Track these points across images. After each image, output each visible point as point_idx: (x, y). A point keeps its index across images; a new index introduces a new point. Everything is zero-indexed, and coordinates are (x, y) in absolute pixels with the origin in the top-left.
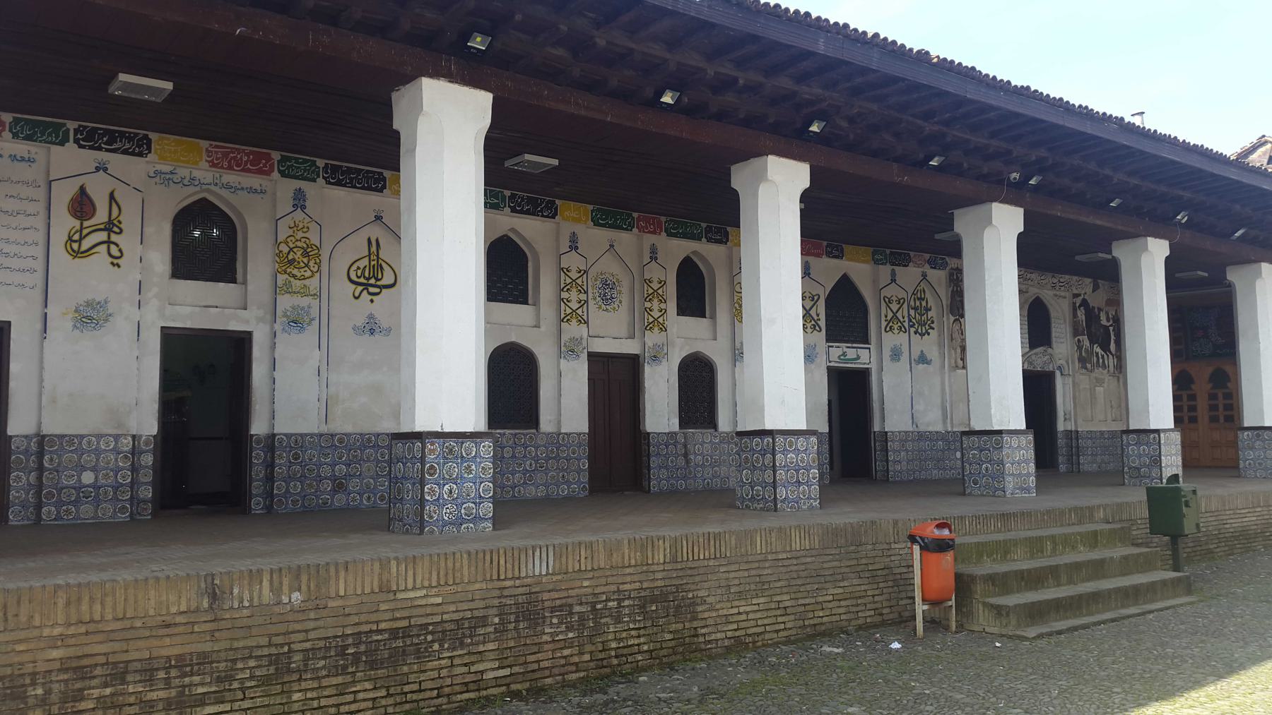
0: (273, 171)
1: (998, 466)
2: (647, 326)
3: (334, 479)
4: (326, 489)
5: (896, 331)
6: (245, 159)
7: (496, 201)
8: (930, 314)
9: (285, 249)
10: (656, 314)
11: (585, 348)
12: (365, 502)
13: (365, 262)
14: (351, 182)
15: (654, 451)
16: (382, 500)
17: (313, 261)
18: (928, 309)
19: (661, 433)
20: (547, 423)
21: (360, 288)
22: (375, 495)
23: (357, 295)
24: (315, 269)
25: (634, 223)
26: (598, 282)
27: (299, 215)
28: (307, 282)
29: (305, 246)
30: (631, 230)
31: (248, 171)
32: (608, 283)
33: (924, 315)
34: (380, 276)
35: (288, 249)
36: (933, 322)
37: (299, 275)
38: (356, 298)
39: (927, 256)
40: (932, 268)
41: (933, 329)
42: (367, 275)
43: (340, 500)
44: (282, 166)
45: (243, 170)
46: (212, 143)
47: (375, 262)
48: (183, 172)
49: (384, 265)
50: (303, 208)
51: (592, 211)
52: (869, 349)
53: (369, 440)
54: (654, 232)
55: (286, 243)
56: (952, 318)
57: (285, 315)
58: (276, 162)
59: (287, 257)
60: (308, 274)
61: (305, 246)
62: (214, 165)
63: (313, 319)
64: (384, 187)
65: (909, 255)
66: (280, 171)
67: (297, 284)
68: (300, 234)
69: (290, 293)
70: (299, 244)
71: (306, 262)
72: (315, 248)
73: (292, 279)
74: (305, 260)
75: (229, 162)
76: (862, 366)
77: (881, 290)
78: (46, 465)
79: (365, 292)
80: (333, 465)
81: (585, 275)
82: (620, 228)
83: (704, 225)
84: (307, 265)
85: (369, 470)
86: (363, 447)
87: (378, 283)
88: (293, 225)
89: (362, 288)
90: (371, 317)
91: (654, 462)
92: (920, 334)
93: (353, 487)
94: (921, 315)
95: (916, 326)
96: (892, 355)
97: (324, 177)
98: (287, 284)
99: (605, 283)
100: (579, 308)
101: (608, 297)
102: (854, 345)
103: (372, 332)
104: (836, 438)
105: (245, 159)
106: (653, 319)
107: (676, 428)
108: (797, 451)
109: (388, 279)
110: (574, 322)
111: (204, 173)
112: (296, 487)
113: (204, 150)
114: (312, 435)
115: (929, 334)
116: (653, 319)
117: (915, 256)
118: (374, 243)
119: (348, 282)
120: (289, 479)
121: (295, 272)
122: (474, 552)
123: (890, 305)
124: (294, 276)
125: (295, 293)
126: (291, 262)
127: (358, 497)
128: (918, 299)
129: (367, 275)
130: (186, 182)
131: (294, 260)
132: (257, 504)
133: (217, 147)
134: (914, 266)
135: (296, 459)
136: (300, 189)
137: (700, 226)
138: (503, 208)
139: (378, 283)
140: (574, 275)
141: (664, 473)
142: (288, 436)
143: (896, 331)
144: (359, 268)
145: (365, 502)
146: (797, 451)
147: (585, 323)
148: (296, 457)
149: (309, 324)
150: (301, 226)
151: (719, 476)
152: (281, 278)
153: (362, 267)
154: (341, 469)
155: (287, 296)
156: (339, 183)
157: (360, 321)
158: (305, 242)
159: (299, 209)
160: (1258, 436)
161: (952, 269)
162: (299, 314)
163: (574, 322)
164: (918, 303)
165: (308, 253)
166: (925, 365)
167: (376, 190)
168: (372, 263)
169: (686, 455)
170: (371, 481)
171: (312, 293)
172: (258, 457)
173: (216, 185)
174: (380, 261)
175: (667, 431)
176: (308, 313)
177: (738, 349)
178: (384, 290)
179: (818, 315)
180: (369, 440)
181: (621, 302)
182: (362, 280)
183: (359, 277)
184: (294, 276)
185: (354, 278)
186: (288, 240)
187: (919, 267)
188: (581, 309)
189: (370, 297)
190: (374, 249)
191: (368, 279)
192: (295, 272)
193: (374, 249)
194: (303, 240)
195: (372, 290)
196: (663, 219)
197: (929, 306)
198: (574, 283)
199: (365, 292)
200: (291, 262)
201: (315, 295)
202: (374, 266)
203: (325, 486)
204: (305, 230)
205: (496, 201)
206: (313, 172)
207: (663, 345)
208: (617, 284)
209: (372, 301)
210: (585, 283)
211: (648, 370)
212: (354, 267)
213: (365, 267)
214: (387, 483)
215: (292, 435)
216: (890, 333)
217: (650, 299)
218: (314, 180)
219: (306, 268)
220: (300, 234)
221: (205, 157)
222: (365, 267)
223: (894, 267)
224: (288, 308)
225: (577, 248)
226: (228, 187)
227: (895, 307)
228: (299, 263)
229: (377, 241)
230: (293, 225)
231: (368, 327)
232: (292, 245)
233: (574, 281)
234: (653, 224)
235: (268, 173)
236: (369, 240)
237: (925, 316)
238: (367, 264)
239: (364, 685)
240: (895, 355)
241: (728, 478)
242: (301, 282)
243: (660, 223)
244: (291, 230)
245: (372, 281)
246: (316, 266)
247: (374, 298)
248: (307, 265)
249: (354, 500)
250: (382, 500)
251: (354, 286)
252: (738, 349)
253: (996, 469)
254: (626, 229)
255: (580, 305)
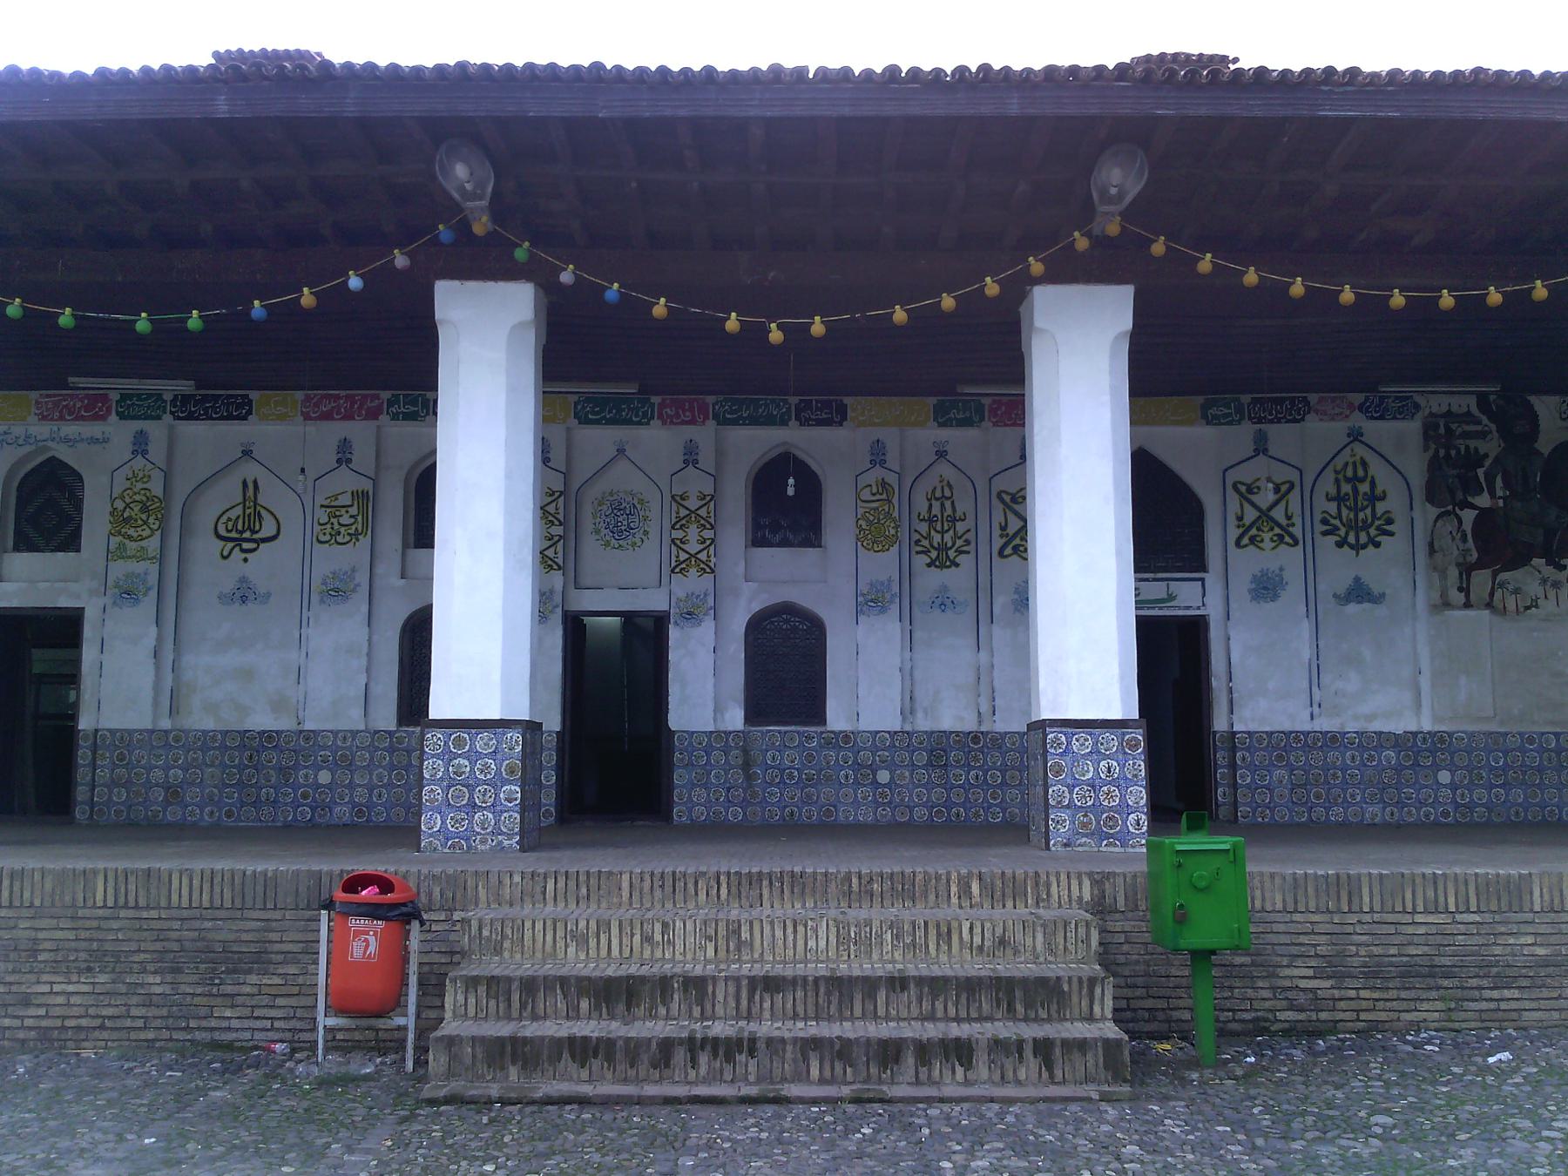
0: (110, 414)
1: (322, 810)
2: (676, 566)
3: (167, 788)
4: (157, 799)
5: (1267, 544)
6: (79, 405)
7: (413, 409)
8: (1381, 507)
9: (120, 505)
10: (693, 547)
11: (557, 606)
12: (206, 818)
13: (238, 511)
14: (206, 413)
15: (682, 760)
16: (229, 817)
17: (154, 516)
18: (1374, 498)
19: (1009, 733)
20: (837, 718)
21: (230, 545)
22: (220, 810)
23: (225, 553)
24: (155, 527)
25: (653, 411)
26: (605, 507)
27: (139, 462)
28: (143, 543)
29: (144, 499)
30: (648, 424)
31: (83, 418)
32: (622, 507)
33: (1363, 509)
34: (257, 528)
35: (124, 505)
36: (1390, 522)
37: (135, 535)
38: (225, 558)
39: (1358, 398)
40: (1373, 418)
41: (1391, 534)
42: (240, 528)
43: (173, 814)
44: (121, 407)
45: (76, 419)
46: (42, 392)
47: (252, 510)
48: (18, 430)
49: (263, 512)
50: (144, 453)
51: (576, 404)
52: (1202, 580)
53: (214, 739)
54: (693, 422)
55: (122, 498)
56: (1434, 512)
57: (117, 586)
58: (114, 405)
59: (122, 515)
60: (147, 532)
61: (144, 499)
62: (44, 418)
63: (149, 589)
64: (250, 412)
65: (1305, 400)
66: (118, 413)
67: (132, 546)
68: (140, 485)
69: (123, 558)
70: (137, 498)
71: (145, 519)
72: (156, 500)
73: (127, 542)
74: (144, 517)
75: (61, 412)
76: (1181, 613)
77: (1226, 470)
78: (1239, 762)
79: (237, 549)
80: (167, 768)
81: (712, 503)
82: (628, 422)
83: (794, 400)
84: (145, 523)
85: (213, 777)
86: (205, 749)
87: (255, 536)
88: (130, 476)
89: (233, 544)
90: (243, 580)
91: (680, 777)
92: (1351, 547)
93: (192, 799)
94: (1356, 509)
95: (1342, 532)
96: (1254, 590)
97: (172, 413)
98: (121, 546)
99: (617, 508)
100: (550, 547)
101: (623, 528)
102: (1160, 575)
103: (244, 599)
104: (567, 737)
105: (79, 405)
106: (687, 556)
107: (735, 718)
108: (474, 756)
109: (268, 529)
110: (693, 571)
111: (42, 430)
112: (120, 795)
113: (34, 402)
114: (141, 732)
115: (1377, 545)
116: (687, 556)
117: (1320, 400)
118: (251, 486)
119: (213, 536)
120: (114, 783)
121: (131, 532)
122: (1461, 879)
123: (1253, 498)
124: (130, 537)
125: (130, 557)
126: (127, 521)
127: (198, 811)
128: (1348, 480)
129: (240, 528)
130: (21, 442)
131: (130, 518)
132: (80, 813)
133: (48, 396)
134: (1321, 420)
135: (121, 760)
136: (142, 432)
137: (785, 402)
138: (424, 417)
139: (255, 536)
140: (693, 503)
141: (700, 794)
142: (112, 732)
143: (1267, 544)
144: (230, 520)
145: (206, 818)
146: (474, 756)
147: (560, 568)
148: (121, 758)
149: (145, 594)
150: (141, 475)
151: (816, 802)
152: (115, 540)
153: (234, 518)
154: (176, 774)
155: (121, 562)
156: (191, 417)
157: (229, 585)
158: (145, 495)
159: (140, 456)
160: (459, 743)
161: (1432, 414)
162: (132, 582)
163: (693, 571)
164: (936, 510)
165: (147, 507)
166: (1366, 605)
167: (238, 418)
168: (248, 511)
169: (747, 765)
170: (215, 791)
171: (150, 556)
172: (83, 755)
173: (53, 440)
174: (258, 508)
175: (711, 728)
176: (144, 582)
177: (863, 595)
178: (262, 545)
179: (1289, 518)
180: (214, 739)
181: (646, 533)
182: (234, 535)
183: (228, 531)
184: (130, 537)
185: (222, 532)
186: (125, 494)
187: (1333, 419)
188: (552, 549)
189: (244, 555)
190: (250, 492)
191: (242, 532)
192: (131, 532)
193: (250, 492)
194: (143, 492)
195: (246, 546)
196: (711, 399)
197: (1378, 491)
198: (693, 515)
199: (237, 549)
200: (127, 521)
201: (154, 558)
202: (249, 515)
203: (156, 794)
204: (145, 480)
205: (413, 409)
206: (159, 408)
207: (706, 595)
208: (639, 506)
209: (246, 560)
210: (712, 514)
211: (674, 633)
212: (224, 519)
213: (238, 517)
214: (236, 795)
215: (118, 730)
216: (1252, 547)
217: (684, 525)
218: (159, 418)
219: (145, 527)
220: (140, 485)
221: (33, 410)
222: (238, 517)
223: (1262, 426)
224: (120, 576)
225: (695, 462)
226: (67, 440)
227: (1266, 497)
228: (136, 520)
229: (255, 482)
230: (130, 476)
231: (238, 595)
232: (128, 500)
233: (693, 512)
234: (691, 409)
235: (103, 418)
236: (245, 484)
237: (1369, 511)
238: (241, 512)
239: (855, 1031)
240: (1265, 588)
241: (834, 806)
242: (140, 543)
243: (703, 409)
244: (129, 482)
245: (247, 535)
246: (157, 522)
247: (247, 555)
248: (145, 523)
249: (192, 813)
250: (229, 817)
251: (223, 543)
252: (863, 595)
253: (882, 815)
254: (639, 423)
255: (551, 542)
